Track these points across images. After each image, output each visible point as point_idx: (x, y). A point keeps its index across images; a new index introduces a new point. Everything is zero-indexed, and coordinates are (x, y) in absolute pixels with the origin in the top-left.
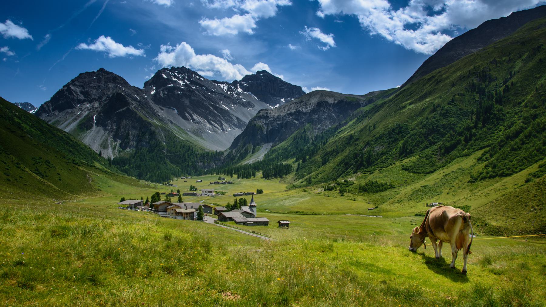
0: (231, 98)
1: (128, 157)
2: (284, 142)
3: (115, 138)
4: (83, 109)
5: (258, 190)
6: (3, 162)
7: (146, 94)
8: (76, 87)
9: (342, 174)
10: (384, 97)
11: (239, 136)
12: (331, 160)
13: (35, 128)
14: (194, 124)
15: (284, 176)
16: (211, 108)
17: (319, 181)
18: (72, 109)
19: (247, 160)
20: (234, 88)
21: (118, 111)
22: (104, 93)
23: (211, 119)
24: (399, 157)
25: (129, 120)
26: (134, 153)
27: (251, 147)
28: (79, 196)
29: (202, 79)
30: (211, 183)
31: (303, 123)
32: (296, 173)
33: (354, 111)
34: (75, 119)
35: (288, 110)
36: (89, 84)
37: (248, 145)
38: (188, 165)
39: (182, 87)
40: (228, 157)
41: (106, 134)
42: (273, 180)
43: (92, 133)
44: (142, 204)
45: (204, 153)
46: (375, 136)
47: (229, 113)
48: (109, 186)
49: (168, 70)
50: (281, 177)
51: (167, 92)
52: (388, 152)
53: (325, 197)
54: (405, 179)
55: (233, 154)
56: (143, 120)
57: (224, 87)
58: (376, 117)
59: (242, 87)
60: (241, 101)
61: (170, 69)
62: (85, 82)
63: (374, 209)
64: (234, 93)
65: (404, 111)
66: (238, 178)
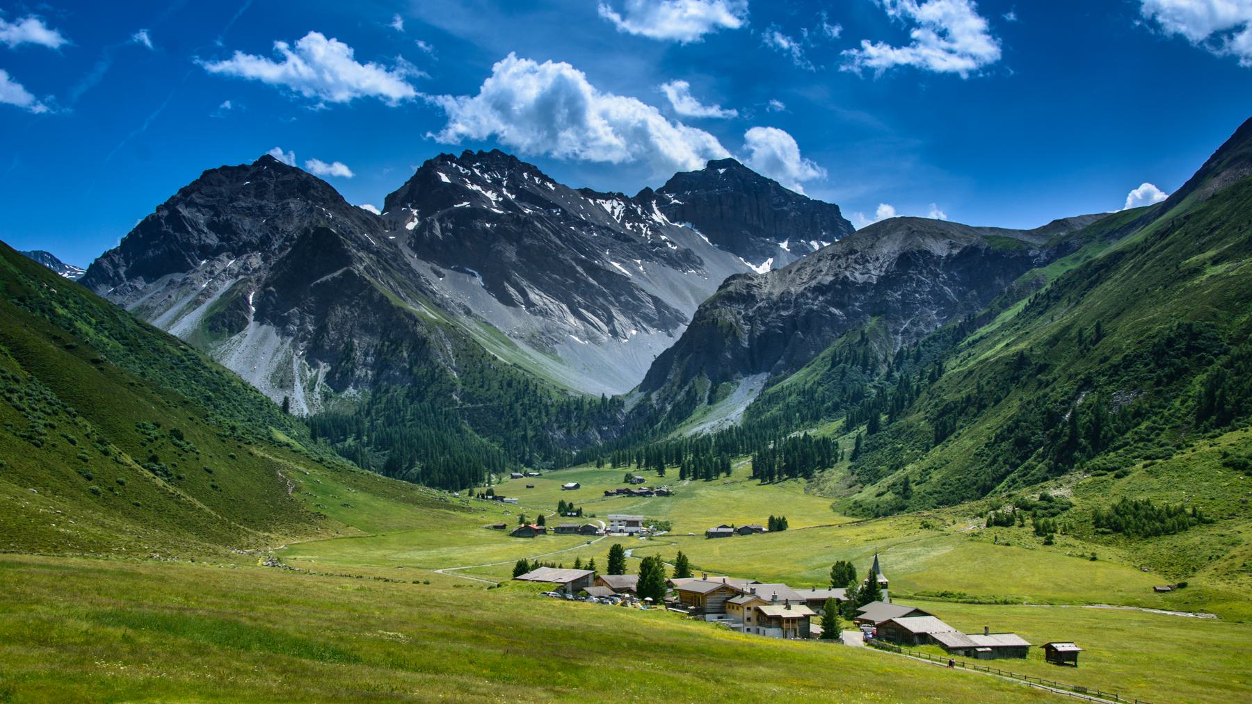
0: (634, 241)
1: (350, 412)
2: (802, 373)
3: (313, 356)
4: (216, 273)
5: (772, 520)
6: (66, 437)
7: (393, 230)
8: (195, 210)
9: (1008, 473)
10: (1106, 236)
11: (667, 354)
12: (961, 427)
13: (106, 333)
14: (533, 317)
15: (817, 473)
16: (579, 269)
17: (936, 492)
18: (184, 272)
19: (694, 424)
20: (643, 213)
21: (318, 281)
22: (277, 229)
23: (579, 302)
24: (1197, 426)
25: (353, 306)
26: (367, 400)
27: (704, 385)
28: (273, 536)
29: (550, 186)
30: (607, 494)
31: (857, 315)
32: (851, 464)
33: (1014, 279)
34: (196, 303)
35: (812, 278)
36: (231, 201)
37: (695, 379)
38: (524, 437)
39: (496, 211)
40: (640, 414)
41: (286, 346)
42: (785, 483)
43: (246, 341)
44: (591, 580)
45: (569, 404)
46: (1106, 359)
47: (630, 284)
48: (345, 505)
49: (453, 161)
50: (807, 476)
51: (452, 223)
52: (1157, 410)
53: (999, 547)
54: (1239, 497)
55: (651, 406)
56: (392, 307)
57: (614, 208)
58: (1099, 298)
59: (665, 207)
60: (663, 249)
61: (458, 157)
62: (221, 196)
63: (1173, 589)
64: (642, 225)
65: (1196, 282)
66: (682, 477)
